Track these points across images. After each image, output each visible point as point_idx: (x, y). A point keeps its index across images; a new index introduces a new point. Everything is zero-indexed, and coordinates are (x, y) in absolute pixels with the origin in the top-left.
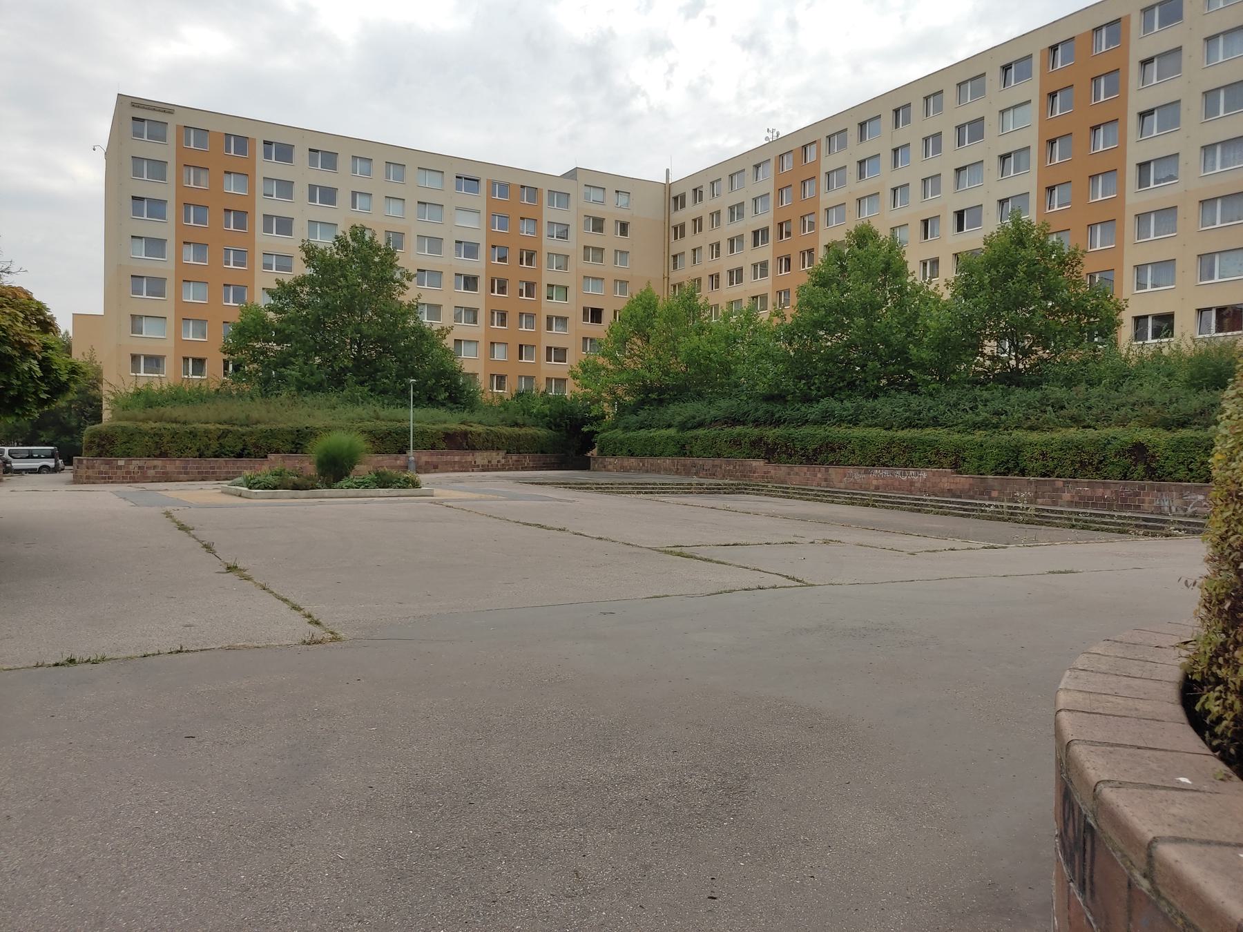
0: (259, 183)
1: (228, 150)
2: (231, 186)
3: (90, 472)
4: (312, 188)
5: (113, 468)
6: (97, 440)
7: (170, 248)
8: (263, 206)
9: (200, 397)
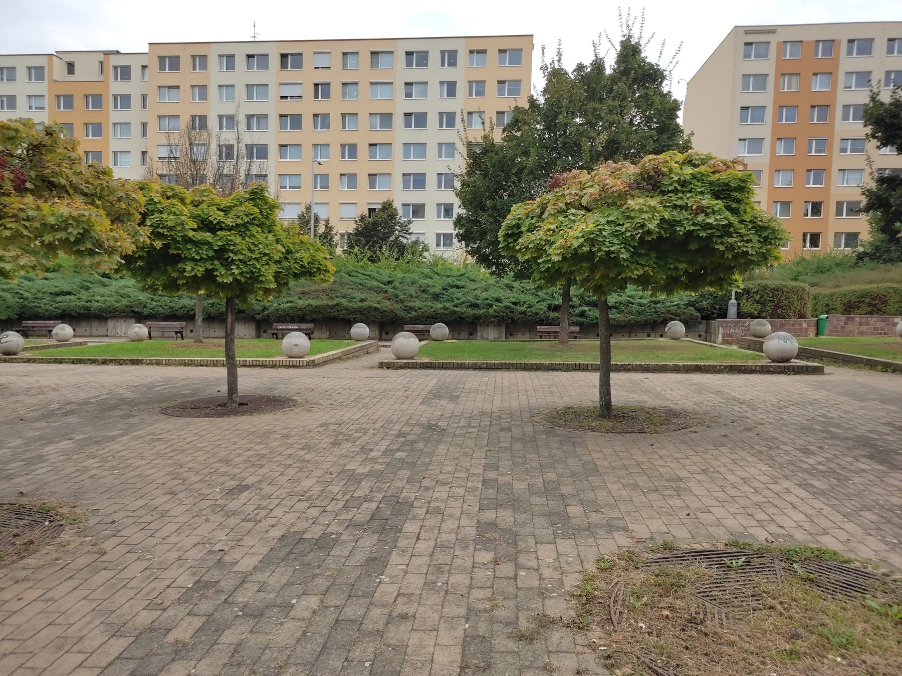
1: (817, 55)
2: (818, 85)
3: (864, 328)
5: (889, 325)
6: (867, 300)
9: (822, 269)
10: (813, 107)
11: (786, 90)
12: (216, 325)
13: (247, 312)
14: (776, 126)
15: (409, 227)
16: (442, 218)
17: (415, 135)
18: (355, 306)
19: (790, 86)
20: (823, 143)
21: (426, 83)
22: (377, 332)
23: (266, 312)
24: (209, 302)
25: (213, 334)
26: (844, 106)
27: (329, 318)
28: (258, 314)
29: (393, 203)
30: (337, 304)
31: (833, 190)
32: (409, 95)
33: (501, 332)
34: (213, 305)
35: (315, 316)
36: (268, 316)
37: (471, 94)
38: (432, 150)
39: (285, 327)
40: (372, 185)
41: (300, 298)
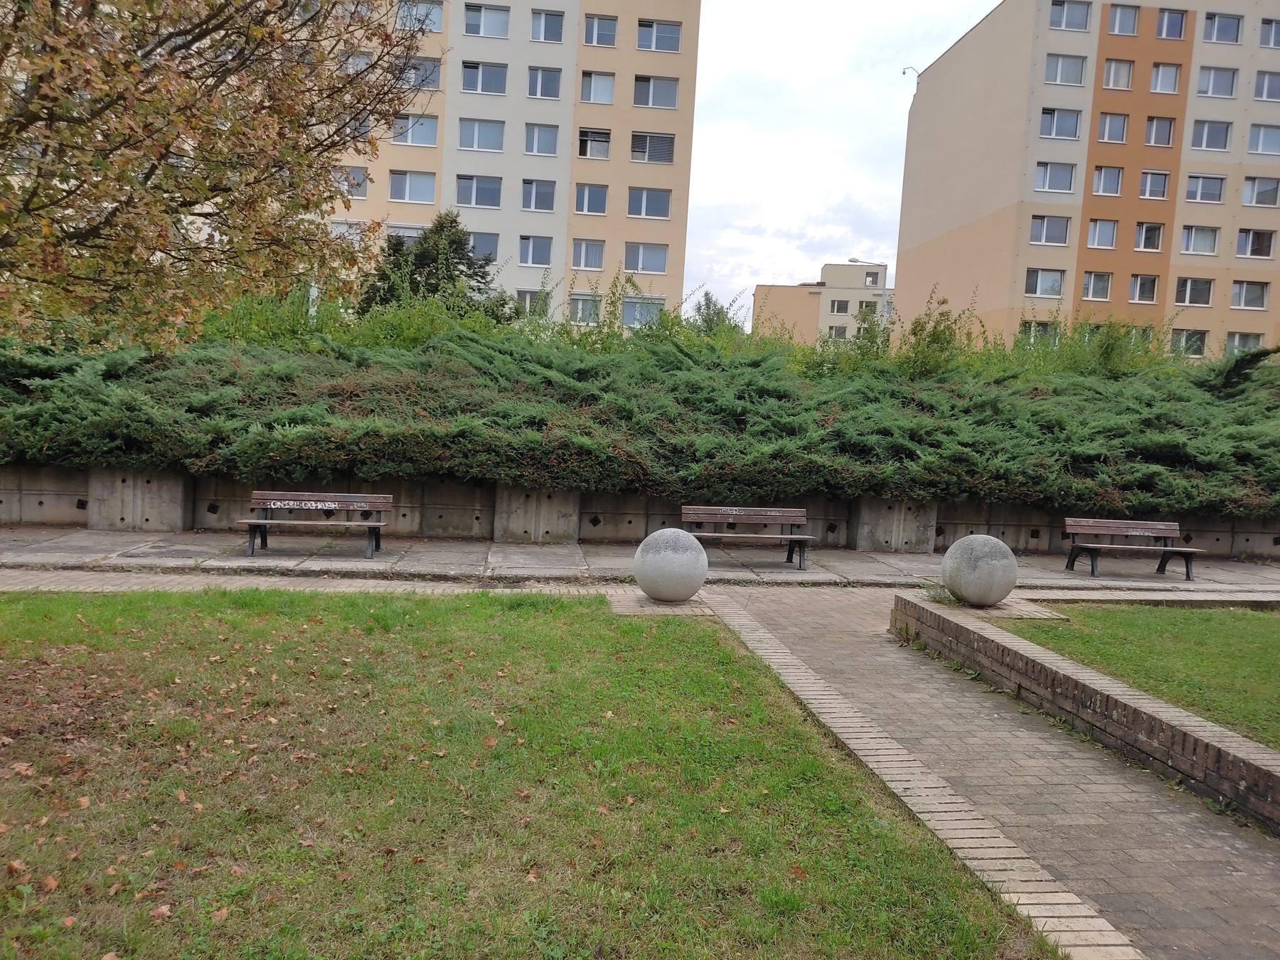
0: (1195, 73)
1: (1160, 33)
2: (1162, 83)
4: (635, 193)
7: (1080, 176)
8: (1200, 107)
10: (1151, 119)
11: (1111, 86)
12: (47, 485)
13: (157, 447)
14: (1095, 142)
15: (487, 269)
16: (530, 264)
17: (482, 105)
18: (516, 441)
19: (1118, 79)
20: (1163, 180)
21: (506, 9)
22: (575, 518)
23: (223, 451)
24: (21, 410)
25: (32, 512)
26: (1197, 122)
27: (434, 474)
28: (197, 456)
29: (459, 219)
30: (462, 434)
31: (1174, 260)
32: (472, 29)
33: (926, 527)
34: (34, 421)
35: (389, 467)
36: (230, 462)
37: (589, 39)
38: (514, 135)
39: (292, 504)
40: (397, 192)
41: (331, 410)
